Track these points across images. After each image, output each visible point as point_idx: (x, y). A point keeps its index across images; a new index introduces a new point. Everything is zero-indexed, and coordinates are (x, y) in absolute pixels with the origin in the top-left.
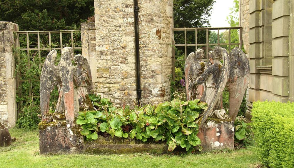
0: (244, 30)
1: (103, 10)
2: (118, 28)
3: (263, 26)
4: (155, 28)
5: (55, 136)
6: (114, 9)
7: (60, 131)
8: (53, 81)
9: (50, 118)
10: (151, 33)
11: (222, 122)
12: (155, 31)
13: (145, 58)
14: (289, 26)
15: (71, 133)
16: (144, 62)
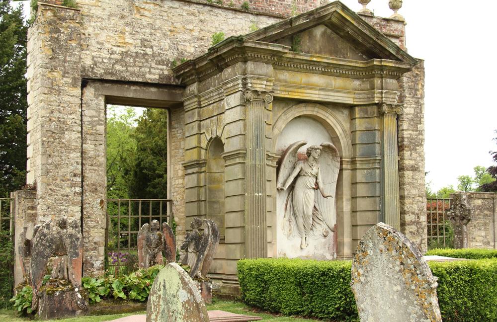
0: (175, 203)
1: (50, 179)
2: (66, 197)
3: (205, 200)
4: (99, 198)
5: (63, 301)
6: (62, 178)
7: (68, 296)
8: (52, 249)
9: (56, 284)
10: (95, 203)
11: (203, 281)
12: (99, 202)
13: (87, 229)
14: (245, 203)
15: (80, 296)
16: (87, 234)
